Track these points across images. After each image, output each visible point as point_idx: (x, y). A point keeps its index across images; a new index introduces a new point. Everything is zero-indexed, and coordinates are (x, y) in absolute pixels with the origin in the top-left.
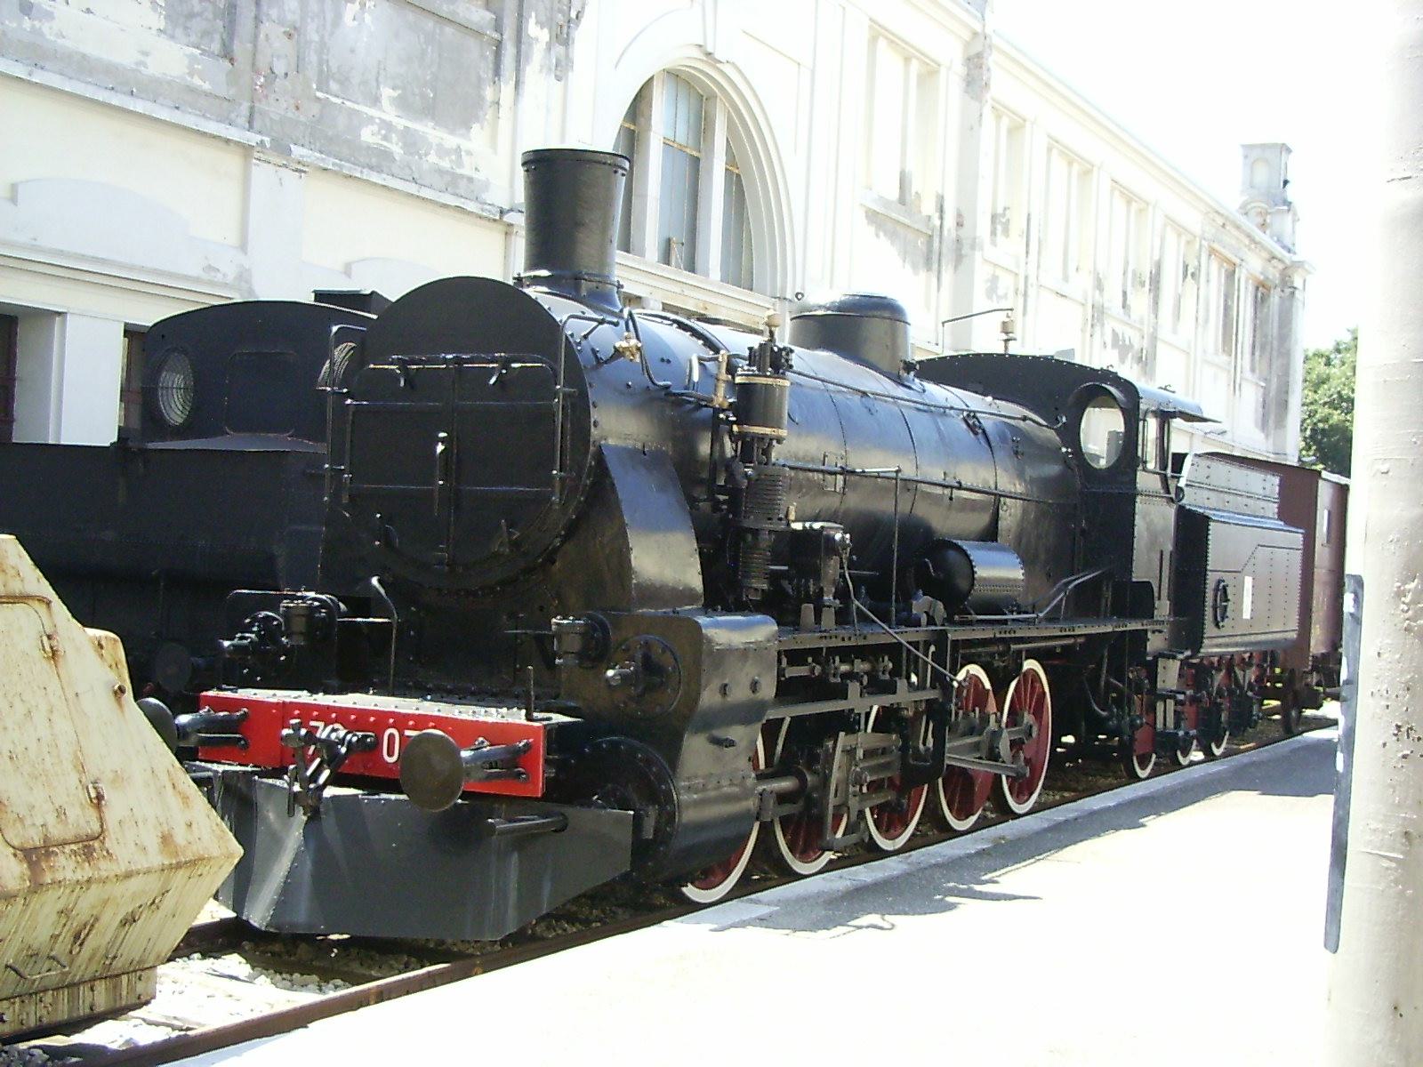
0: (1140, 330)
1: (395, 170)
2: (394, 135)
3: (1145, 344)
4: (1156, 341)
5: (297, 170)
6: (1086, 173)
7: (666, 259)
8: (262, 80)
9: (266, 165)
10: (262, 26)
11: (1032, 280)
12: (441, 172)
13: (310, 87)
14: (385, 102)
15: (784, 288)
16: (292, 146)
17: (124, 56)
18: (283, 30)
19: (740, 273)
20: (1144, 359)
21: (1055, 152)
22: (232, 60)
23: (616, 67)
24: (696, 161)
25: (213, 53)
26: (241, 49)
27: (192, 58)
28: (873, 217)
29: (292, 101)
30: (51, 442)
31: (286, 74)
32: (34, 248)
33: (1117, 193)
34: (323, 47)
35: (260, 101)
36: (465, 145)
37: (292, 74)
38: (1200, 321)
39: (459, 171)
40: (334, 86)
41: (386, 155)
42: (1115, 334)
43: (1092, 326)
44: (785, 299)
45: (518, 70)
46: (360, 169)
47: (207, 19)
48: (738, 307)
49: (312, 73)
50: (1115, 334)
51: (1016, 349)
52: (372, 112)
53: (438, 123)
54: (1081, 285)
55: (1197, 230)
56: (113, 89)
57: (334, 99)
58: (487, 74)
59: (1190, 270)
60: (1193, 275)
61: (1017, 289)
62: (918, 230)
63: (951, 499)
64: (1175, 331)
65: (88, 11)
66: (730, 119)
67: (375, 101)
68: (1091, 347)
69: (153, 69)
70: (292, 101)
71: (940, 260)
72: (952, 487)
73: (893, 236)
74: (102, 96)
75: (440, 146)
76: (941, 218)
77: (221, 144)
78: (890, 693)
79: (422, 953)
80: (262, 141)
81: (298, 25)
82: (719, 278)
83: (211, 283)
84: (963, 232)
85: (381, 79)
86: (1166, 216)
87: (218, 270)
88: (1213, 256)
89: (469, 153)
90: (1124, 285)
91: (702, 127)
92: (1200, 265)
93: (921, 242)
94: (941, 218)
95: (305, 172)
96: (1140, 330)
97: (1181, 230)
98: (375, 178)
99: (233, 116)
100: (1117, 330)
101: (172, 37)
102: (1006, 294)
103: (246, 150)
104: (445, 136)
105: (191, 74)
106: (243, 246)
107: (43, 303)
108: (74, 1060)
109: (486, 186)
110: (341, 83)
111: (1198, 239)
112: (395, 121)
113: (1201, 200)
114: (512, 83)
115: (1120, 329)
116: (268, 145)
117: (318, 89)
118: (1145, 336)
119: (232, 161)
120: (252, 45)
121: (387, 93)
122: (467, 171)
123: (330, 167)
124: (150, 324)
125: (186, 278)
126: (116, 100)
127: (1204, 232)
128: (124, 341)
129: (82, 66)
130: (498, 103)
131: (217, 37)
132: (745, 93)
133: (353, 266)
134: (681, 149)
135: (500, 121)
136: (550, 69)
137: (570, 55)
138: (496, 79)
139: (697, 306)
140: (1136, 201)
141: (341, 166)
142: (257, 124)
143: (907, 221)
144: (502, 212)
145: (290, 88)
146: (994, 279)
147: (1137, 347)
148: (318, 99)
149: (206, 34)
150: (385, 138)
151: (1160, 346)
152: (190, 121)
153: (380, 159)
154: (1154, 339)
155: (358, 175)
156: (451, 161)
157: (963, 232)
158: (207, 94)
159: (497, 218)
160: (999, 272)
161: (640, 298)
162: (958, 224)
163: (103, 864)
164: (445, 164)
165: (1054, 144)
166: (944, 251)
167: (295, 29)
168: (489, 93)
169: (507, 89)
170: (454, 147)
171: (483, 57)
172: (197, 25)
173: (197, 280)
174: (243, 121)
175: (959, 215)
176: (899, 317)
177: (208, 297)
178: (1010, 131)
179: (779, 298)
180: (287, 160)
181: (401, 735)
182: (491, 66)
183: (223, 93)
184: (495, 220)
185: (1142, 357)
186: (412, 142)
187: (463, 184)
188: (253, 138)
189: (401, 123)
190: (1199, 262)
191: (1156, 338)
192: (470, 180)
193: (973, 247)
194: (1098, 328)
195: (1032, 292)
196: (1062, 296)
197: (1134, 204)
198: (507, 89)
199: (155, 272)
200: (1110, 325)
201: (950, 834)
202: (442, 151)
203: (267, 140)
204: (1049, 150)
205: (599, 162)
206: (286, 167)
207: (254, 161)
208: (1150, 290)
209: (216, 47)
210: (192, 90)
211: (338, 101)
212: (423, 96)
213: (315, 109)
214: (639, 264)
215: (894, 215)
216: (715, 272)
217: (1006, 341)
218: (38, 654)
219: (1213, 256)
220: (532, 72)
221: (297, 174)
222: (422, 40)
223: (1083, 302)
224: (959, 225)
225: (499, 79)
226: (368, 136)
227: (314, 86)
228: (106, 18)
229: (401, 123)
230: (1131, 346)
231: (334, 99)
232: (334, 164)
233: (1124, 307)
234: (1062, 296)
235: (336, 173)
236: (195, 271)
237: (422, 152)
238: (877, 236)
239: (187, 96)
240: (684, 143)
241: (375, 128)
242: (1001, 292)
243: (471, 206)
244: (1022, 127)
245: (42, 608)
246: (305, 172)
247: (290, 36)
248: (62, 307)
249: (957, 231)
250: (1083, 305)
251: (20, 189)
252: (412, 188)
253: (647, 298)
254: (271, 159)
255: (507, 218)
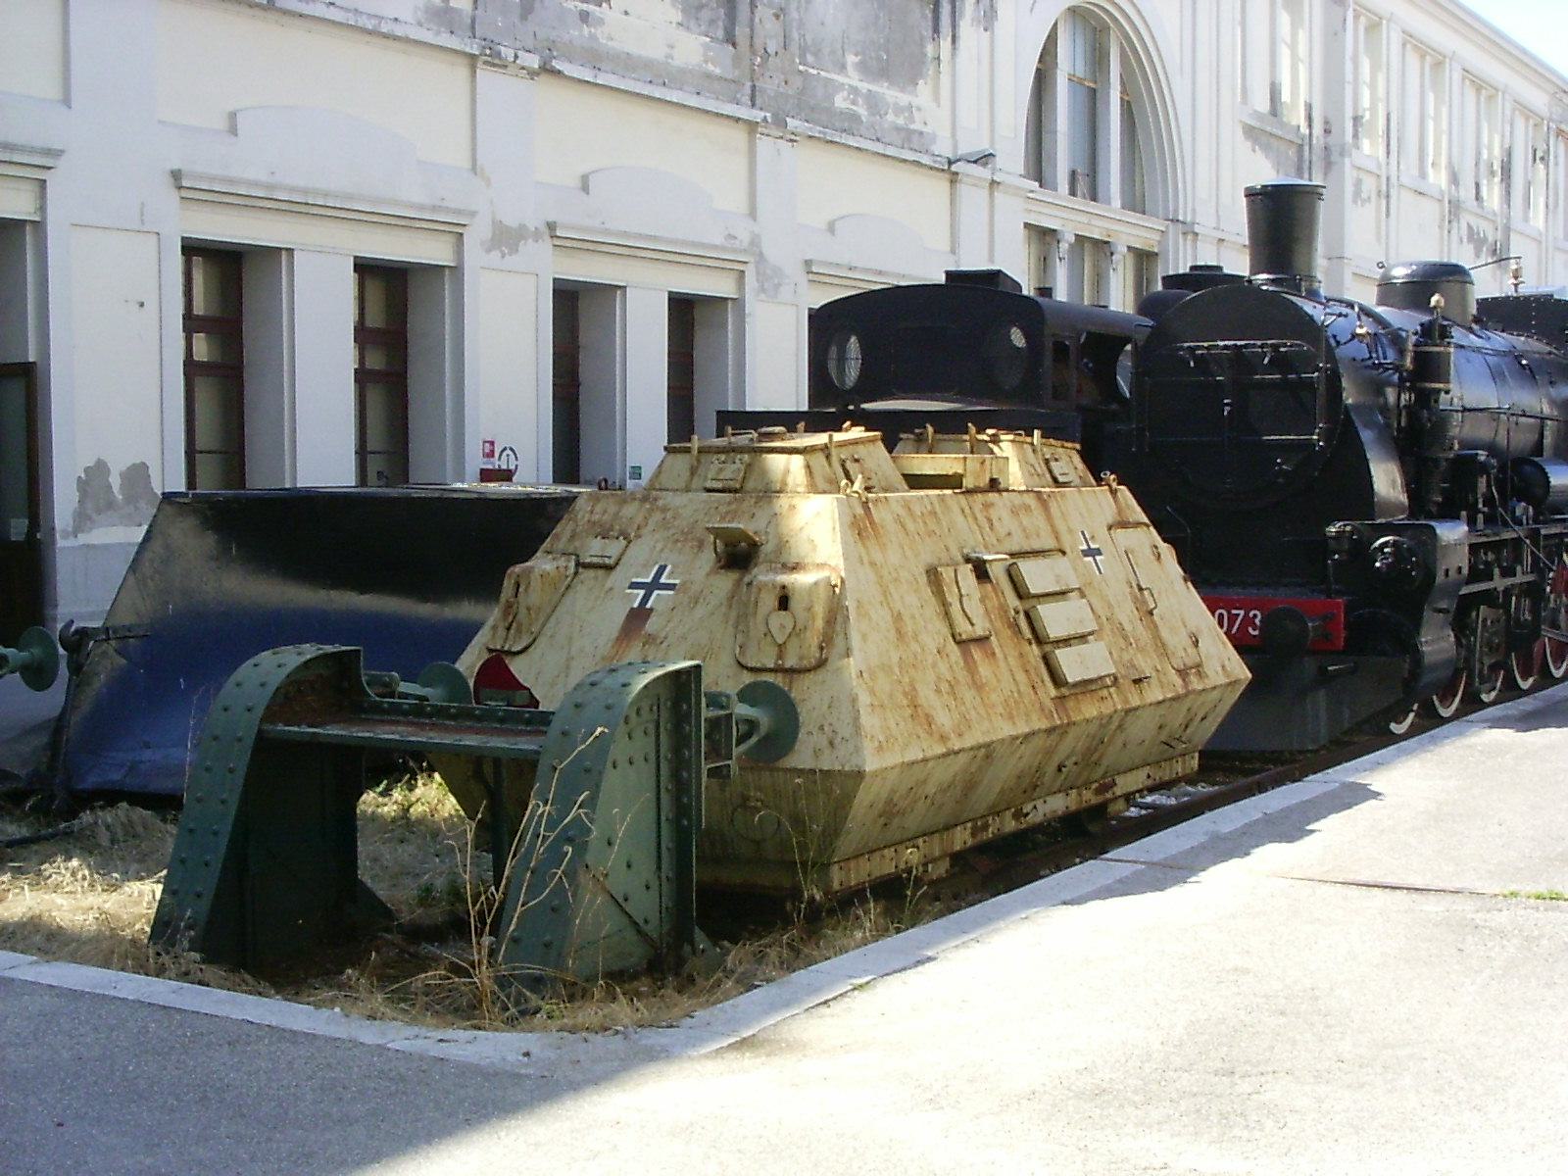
0: (1493, 221)
1: (863, 131)
2: (859, 99)
3: (1499, 235)
4: (1509, 231)
5: (792, 141)
6: (1438, 65)
7: (1073, 193)
8: (759, 59)
9: (766, 138)
10: (756, 11)
11: (1394, 180)
12: (898, 129)
13: (794, 61)
14: (850, 69)
15: (1176, 211)
16: (787, 119)
17: (654, 51)
18: (772, 12)
19: (1135, 202)
20: (1498, 252)
21: (1408, 46)
22: (734, 45)
23: (1032, 10)
24: (1093, 93)
25: (718, 39)
26: (741, 32)
27: (706, 47)
28: (1250, 132)
29: (782, 77)
30: (730, 409)
31: (776, 53)
32: (607, 232)
33: (1467, 82)
34: (801, 24)
35: (758, 79)
36: (916, 102)
37: (781, 51)
38: (1551, 207)
39: (912, 127)
40: (810, 58)
41: (855, 118)
42: (1470, 227)
43: (1450, 222)
44: (1178, 221)
45: (954, 26)
46: (839, 134)
47: (712, 9)
48: (1065, 215)
49: (794, 48)
50: (1470, 227)
51: (1525, 290)
52: (840, 79)
53: (892, 83)
54: (1438, 179)
55: (1544, 111)
56: (651, 82)
57: (811, 71)
58: (928, 33)
59: (1539, 154)
60: (1542, 159)
61: (1380, 191)
62: (1290, 141)
63: (1517, 424)
64: (1526, 219)
65: (626, 13)
66: (1122, 49)
67: (843, 68)
68: (1387, 226)
69: (679, 60)
70: (782, 77)
71: (1310, 168)
72: (1518, 415)
73: (1266, 149)
74: (647, 90)
75: (896, 104)
76: (1310, 126)
77: (732, 123)
78: (1511, 577)
79: (1275, 758)
80: (765, 117)
81: (783, 6)
82: (1119, 206)
83: (734, 251)
84: (1332, 140)
85: (846, 47)
86: (1515, 101)
87: (736, 238)
88: (1560, 137)
89: (919, 109)
90: (1477, 175)
91: (1098, 59)
92: (1549, 149)
93: (1292, 152)
94: (1310, 126)
95: (795, 141)
96: (1493, 221)
97: (1527, 112)
98: (852, 141)
99: (738, 96)
100: (1472, 224)
101: (688, 28)
102: (1369, 198)
103: (752, 126)
104: (900, 95)
105: (706, 62)
106: (753, 214)
107: (15, 213)
108: (1186, 799)
109: (934, 138)
110: (816, 54)
111: (1545, 122)
112: (860, 85)
113: (1549, 80)
114: (949, 39)
115: (1474, 222)
116: (770, 120)
117: (800, 64)
118: (1499, 228)
119: (739, 136)
120: (748, 30)
121: (851, 59)
122: (917, 126)
123: (817, 135)
124: (817, 307)
125: (715, 247)
126: (657, 92)
127: (1551, 114)
128: (354, 277)
129: (628, 64)
130: (939, 58)
131: (721, 24)
132: (1137, 23)
133: (590, 177)
134: (1080, 82)
135: (941, 76)
136: (980, 21)
137: (995, 5)
138: (936, 36)
139: (1101, 234)
140: (1486, 89)
141: (825, 134)
142: (758, 102)
143: (1280, 133)
144: (950, 163)
145: (780, 65)
146: (1358, 183)
147: (1491, 239)
148: (800, 71)
149: (712, 22)
150: (854, 103)
151: (1513, 236)
152: (711, 105)
153: (850, 123)
154: (1507, 229)
155: (838, 140)
156: (905, 118)
157: (1332, 140)
158: (720, 78)
159: (946, 167)
160: (1363, 176)
161: (1055, 231)
162: (1325, 131)
163: (1206, 681)
164: (901, 121)
165: (1409, 39)
166: (1314, 159)
167: (781, 9)
168: (930, 49)
169: (945, 44)
170: (907, 104)
171: (924, 16)
172: (706, 14)
173: (723, 249)
174: (746, 99)
175: (1326, 122)
176: (1468, 280)
177: (739, 264)
178: (1367, 29)
179: (1172, 220)
180: (783, 132)
181: (1229, 613)
182: (930, 24)
183: (730, 77)
184: (943, 170)
185: (1496, 250)
186: (874, 102)
187: (915, 138)
188: (757, 115)
189: (864, 86)
190: (1548, 145)
191: (1509, 228)
192: (921, 133)
193: (1342, 154)
194: (1455, 224)
195: (1393, 192)
196: (1420, 193)
197: (1484, 91)
198: (945, 44)
199: (694, 244)
200: (1466, 218)
201: (1515, 693)
202: (899, 110)
203: (768, 115)
204: (1404, 45)
205: (1308, 192)
206: (782, 138)
207: (758, 135)
208: (1502, 179)
209: (720, 34)
210: (709, 76)
211: (815, 72)
212: (879, 59)
213: (797, 82)
214: (1054, 197)
215: (1268, 129)
216: (1117, 202)
217: (1516, 285)
218: (1152, 557)
219: (1560, 137)
220: (965, 27)
221: (790, 144)
222: (876, 6)
223: (1440, 198)
224: (1327, 132)
225: (938, 37)
226: (840, 102)
227: (798, 61)
228: (639, 18)
229: (864, 86)
230: (1485, 239)
231: (811, 71)
232: (820, 132)
233: (1477, 199)
234: (1420, 193)
235: (819, 139)
236: (719, 240)
237: (882, 112)
238: (1254, 151)
239: (705, 82)
240: (1082, 76)
241: (845, 93)
242: (1364, 195)
243: (925, 160)
244: (1379, 24)
245: (1145, 528)
246: (795, 141)
247: (777, 17)
248: (622, 281)
249: (1325, 138)
250: (1439, 200)
251: (240, 119)
252: (879, 148)
253: (1062, 231)
254: (771, 133)
255: (954, 168)
